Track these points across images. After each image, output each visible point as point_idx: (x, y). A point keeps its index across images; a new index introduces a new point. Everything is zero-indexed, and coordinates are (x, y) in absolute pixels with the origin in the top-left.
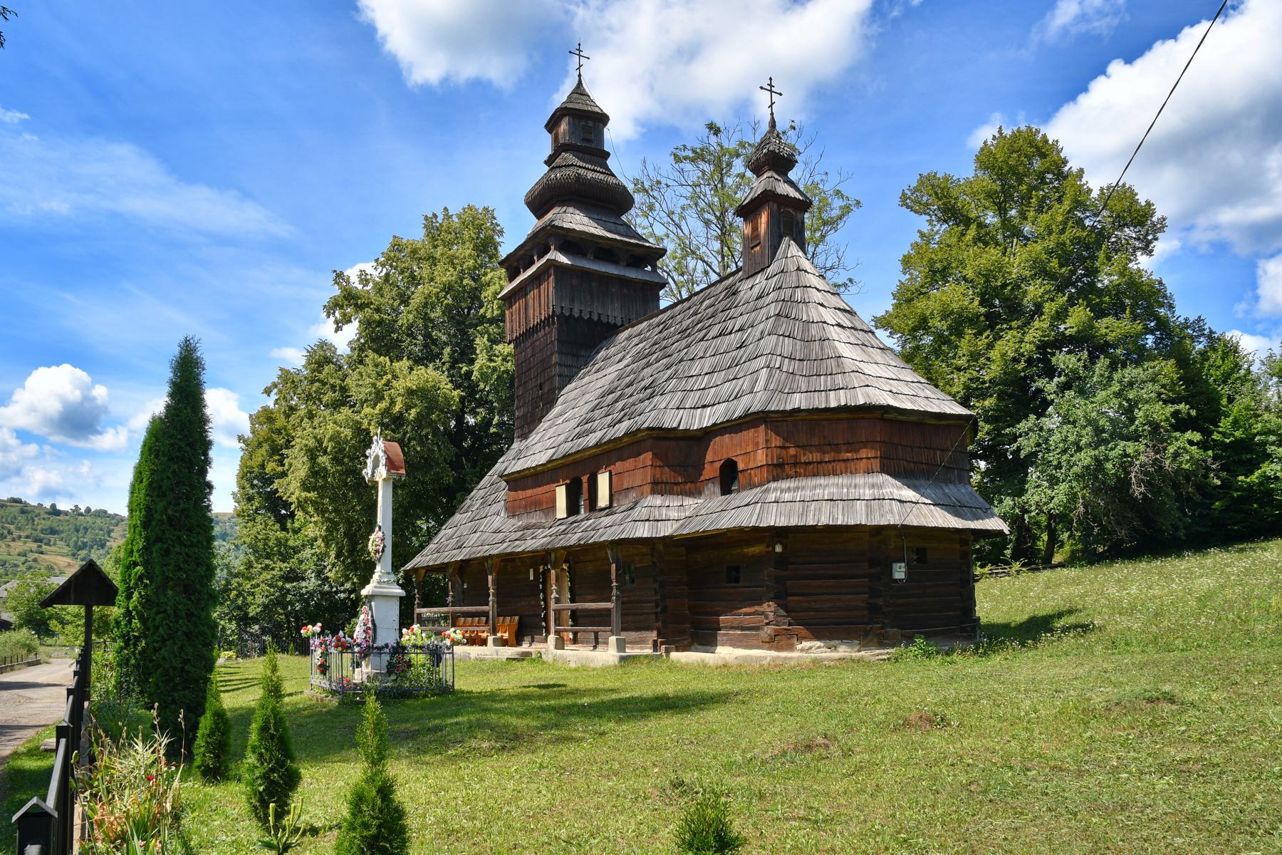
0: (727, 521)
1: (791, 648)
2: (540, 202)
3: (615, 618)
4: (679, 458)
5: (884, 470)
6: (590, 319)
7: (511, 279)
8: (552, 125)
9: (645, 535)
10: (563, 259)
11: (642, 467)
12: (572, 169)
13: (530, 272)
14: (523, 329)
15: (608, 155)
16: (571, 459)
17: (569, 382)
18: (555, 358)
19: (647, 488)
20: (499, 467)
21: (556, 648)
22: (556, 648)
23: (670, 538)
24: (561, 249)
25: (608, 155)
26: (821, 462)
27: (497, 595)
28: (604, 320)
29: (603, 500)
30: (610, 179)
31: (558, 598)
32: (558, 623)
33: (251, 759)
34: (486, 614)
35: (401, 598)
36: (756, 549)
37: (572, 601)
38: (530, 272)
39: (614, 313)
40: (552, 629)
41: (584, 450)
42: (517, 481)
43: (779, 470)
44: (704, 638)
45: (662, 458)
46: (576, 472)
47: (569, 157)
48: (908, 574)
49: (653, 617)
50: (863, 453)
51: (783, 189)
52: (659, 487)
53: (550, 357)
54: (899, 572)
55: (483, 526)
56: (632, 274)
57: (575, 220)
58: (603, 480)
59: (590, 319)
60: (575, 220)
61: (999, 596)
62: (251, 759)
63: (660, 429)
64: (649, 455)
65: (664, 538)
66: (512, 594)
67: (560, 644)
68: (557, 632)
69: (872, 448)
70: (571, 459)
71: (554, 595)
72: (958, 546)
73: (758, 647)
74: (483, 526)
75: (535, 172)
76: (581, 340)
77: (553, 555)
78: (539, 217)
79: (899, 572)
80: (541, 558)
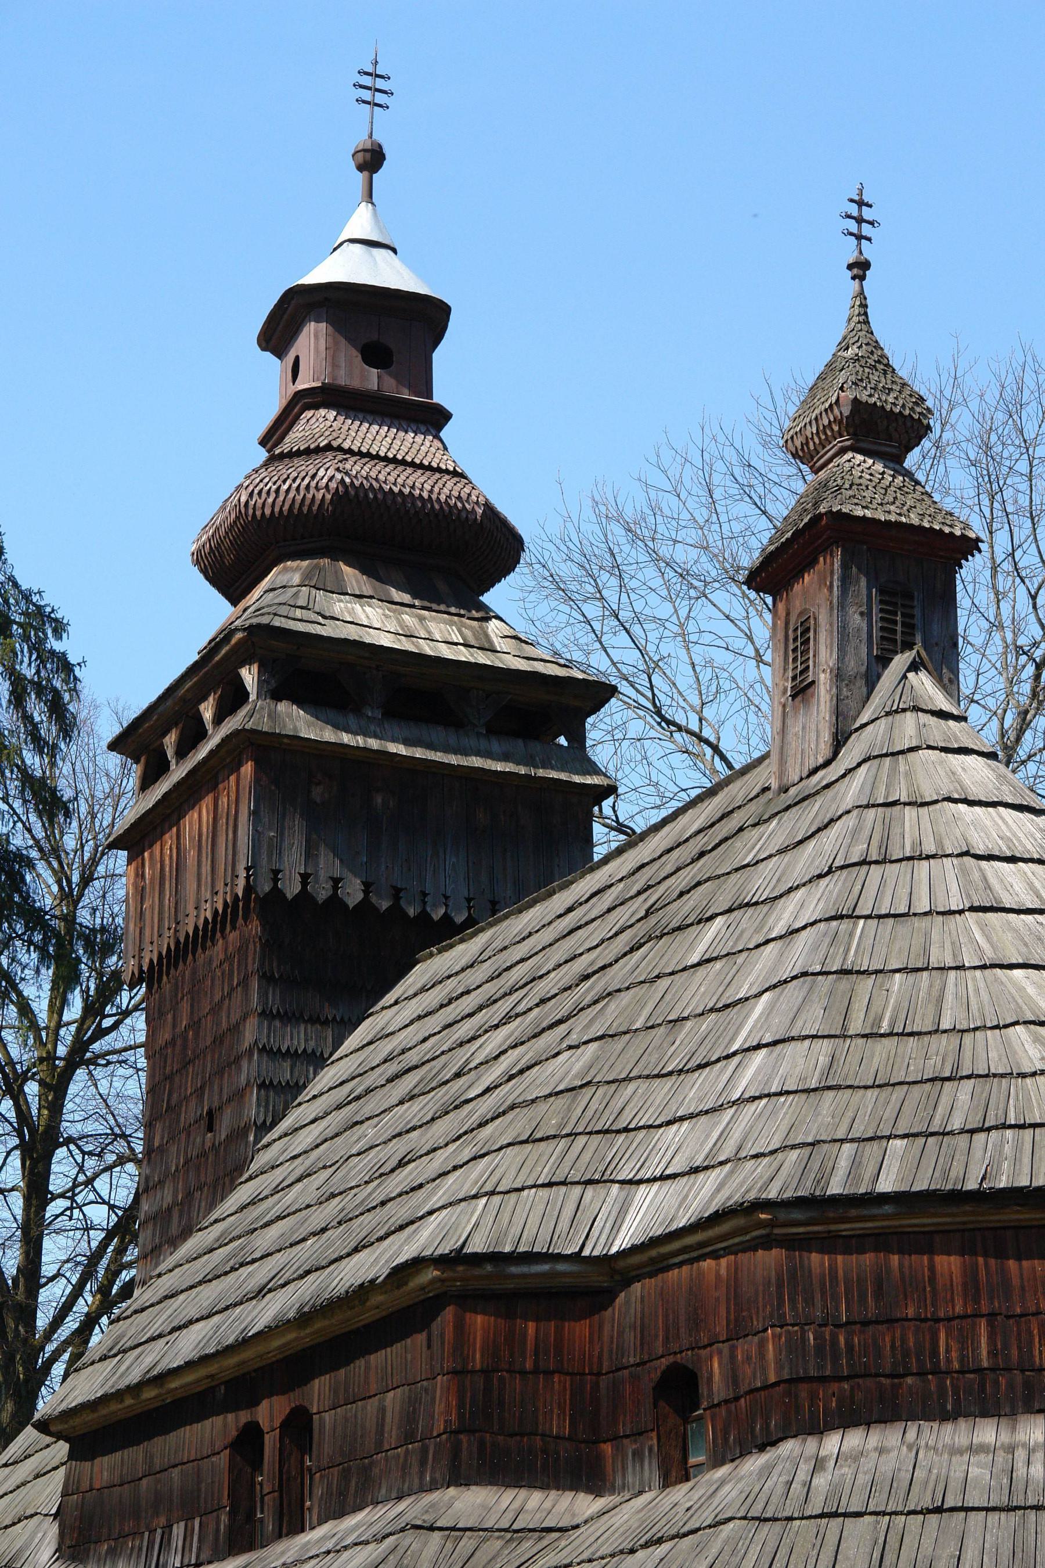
2: (235, 557)
10: (299, 722)
14: (167, 941)
18: (251, 1032)
41: (244, 1343)
47: (319, 424)
53: (236, 1029)
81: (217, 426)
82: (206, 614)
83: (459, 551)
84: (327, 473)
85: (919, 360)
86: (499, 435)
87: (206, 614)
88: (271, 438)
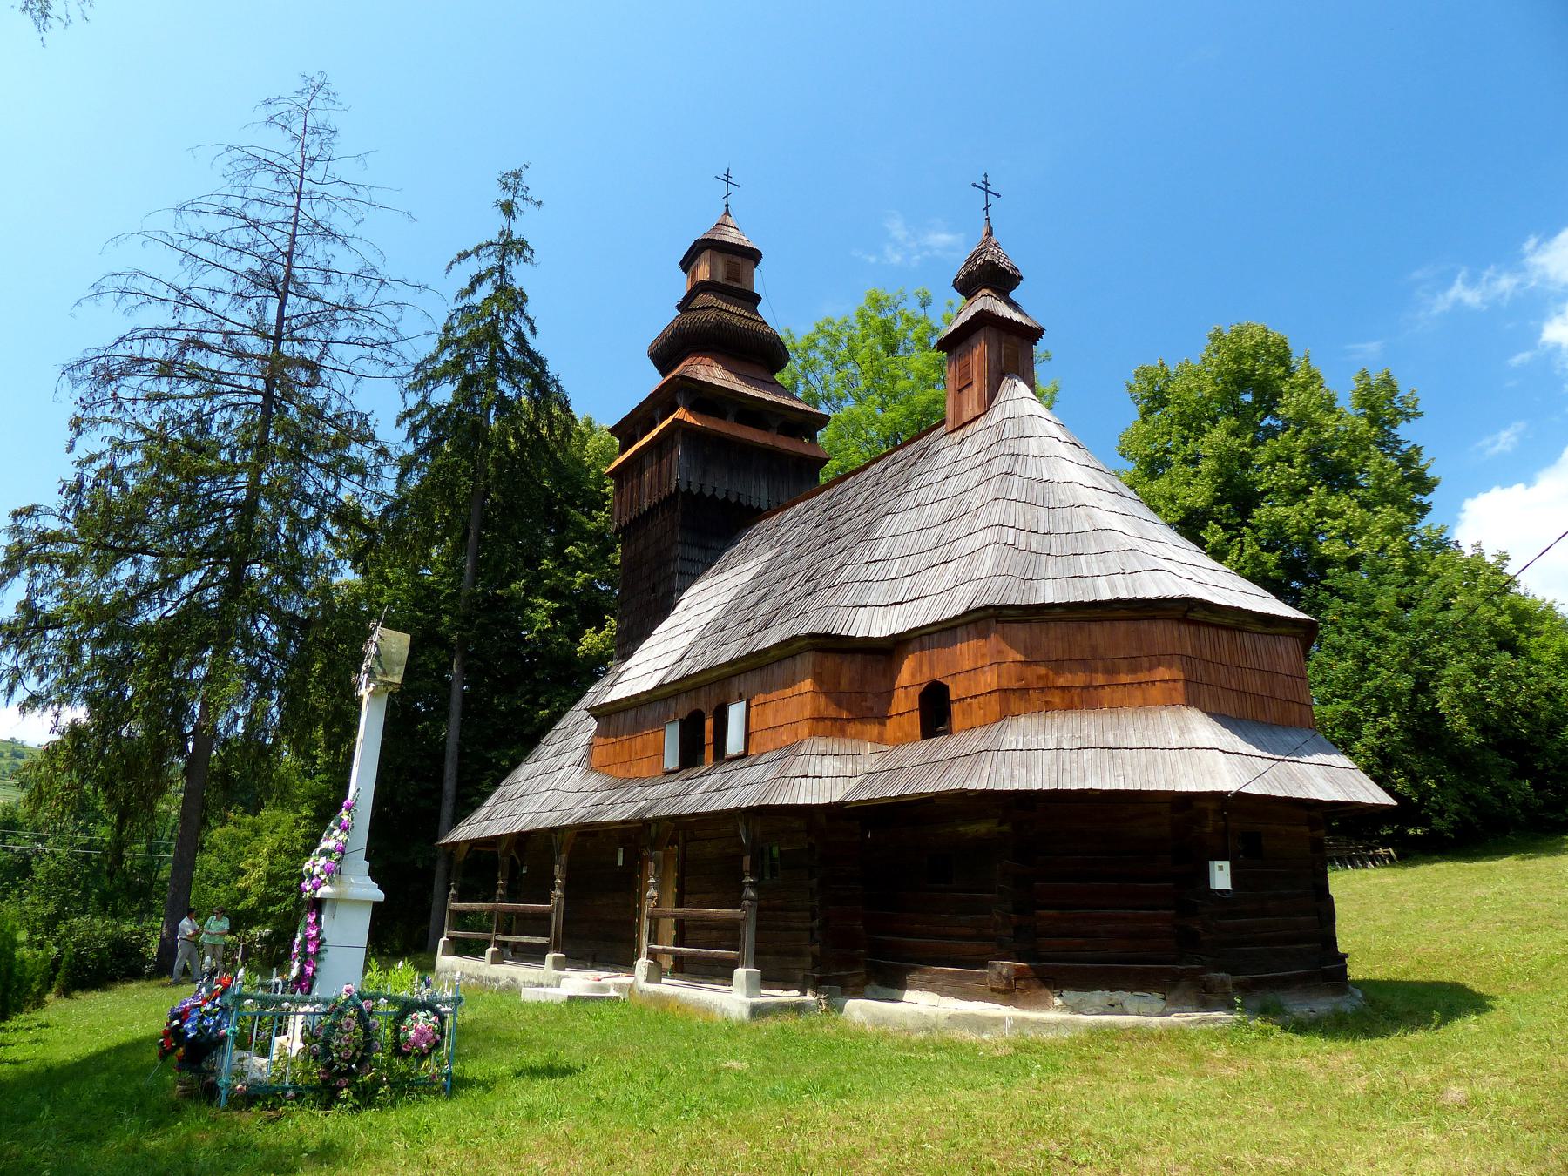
0: (932, 784)
1: (1043, 1004)
2: (666, 354)
3: (749, 936)
4: (854, 677)
5: (1192, 702)
6: (726, 499)
7: (623, 450)
8: (687, 263)
9: (801, 802)
11: (801, 695)
12: (712, 312)
13: (647, 438)
15: (757, 299)
16: (690, 682)
17: (692, 583)
19: (804, 729)
20: (588, 700)
21: (648, 981)
22: (648, 981)
23: (840, 806)
24: (691, 409)
25: (757, 299)
26: (1087, 687)
27: (567, 888)
28: (745, 502)
29: (734, 743)
30: (761, 328)
31: (655, 897)
32: (653, 938)
33: (558, 892)
34: (545, 917)
35: (376, 905)
36: (982, 828)
37: (680, 904)
38: (647, 438)
39: (759, 493)
40: (644, 949)
42: (605, 714)
43: (1014, 700)
44: (887, 977)
45: (827, 686)
46: (693, 715)
47: (703, 299)
48: (1205, 875)
49: (807, 934)
50: (1162, 673)
51: (1003, 310)
52: (830, 725)
54: (1221, 877)
55: (554, 787)
56: (785, 444)
57: (713, 373)
58: (736, 713)
59: (726, 499)
60: (713, 373)
61: (1383, 914)
62: (558, 892)
63: (828, 635)
64: (807, 685)
65: (830, 806)
66: (585, 893)
67: (655, 975)
68: (652, 955)
69: (1171, 666)
70: (690, 682)
71: (652, 892)
72: (1306, 829)
73: (984, 999)
74: (554, 787)
75: (662, 316)
76: (711, 529)
77: (653, 829)
78: (664, 375)
79: (1221, 877)
80: (638, 836)
81: (660, 301)
82: (652, 380)
83: (763, 354)
84: (713, 314)
85: (1011, 254)
86: (786, 306)
87: (652, 380)
88: (684, 306)
